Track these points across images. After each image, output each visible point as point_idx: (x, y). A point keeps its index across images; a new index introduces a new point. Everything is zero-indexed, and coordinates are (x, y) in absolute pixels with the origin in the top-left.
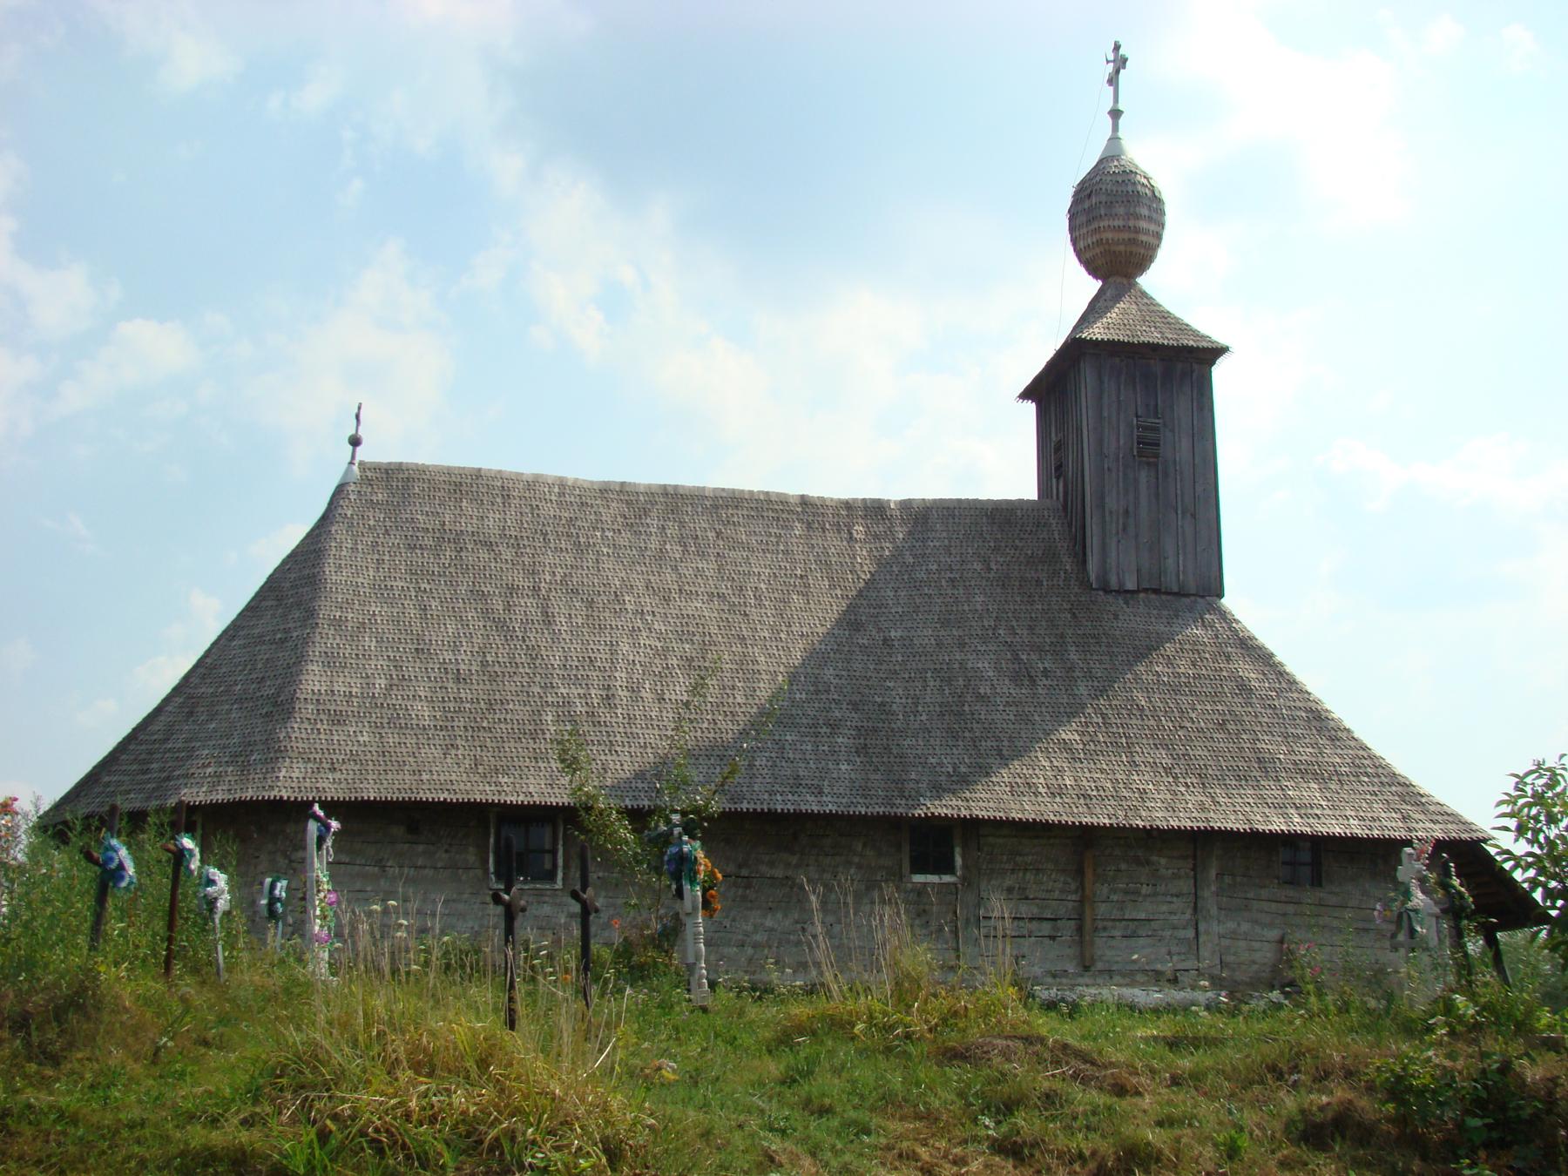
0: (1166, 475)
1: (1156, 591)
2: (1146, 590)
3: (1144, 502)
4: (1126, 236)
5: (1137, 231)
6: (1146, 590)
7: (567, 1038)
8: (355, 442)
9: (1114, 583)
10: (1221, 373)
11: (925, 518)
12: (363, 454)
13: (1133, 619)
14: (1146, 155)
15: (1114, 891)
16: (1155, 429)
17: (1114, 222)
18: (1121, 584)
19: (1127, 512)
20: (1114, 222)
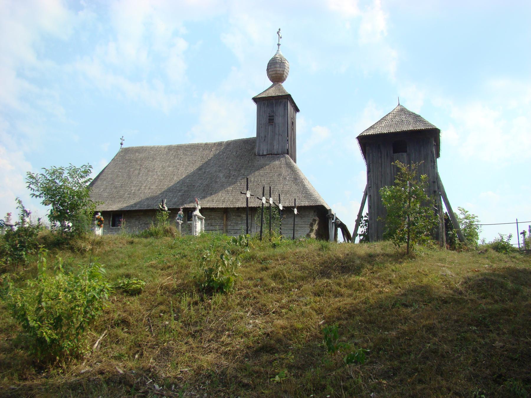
0: (275, 126)
1: (271, 154)
2: (269, 154)
3: (269, 134)
4: (274, 72)
5: (276, 71)
6: (269, 154)
7: (360, 278)
8: (122, 144)
9: (261, 154)
10: (449, 167)
11: (229, 144)
12: (123, 146)
13: (262, 161)
14: (283, 53)
15: (232, 223)
16: (273, 116)
17: (276, 71)
18: (263, 153)
19: (265, 136)
20: (276, 71)
